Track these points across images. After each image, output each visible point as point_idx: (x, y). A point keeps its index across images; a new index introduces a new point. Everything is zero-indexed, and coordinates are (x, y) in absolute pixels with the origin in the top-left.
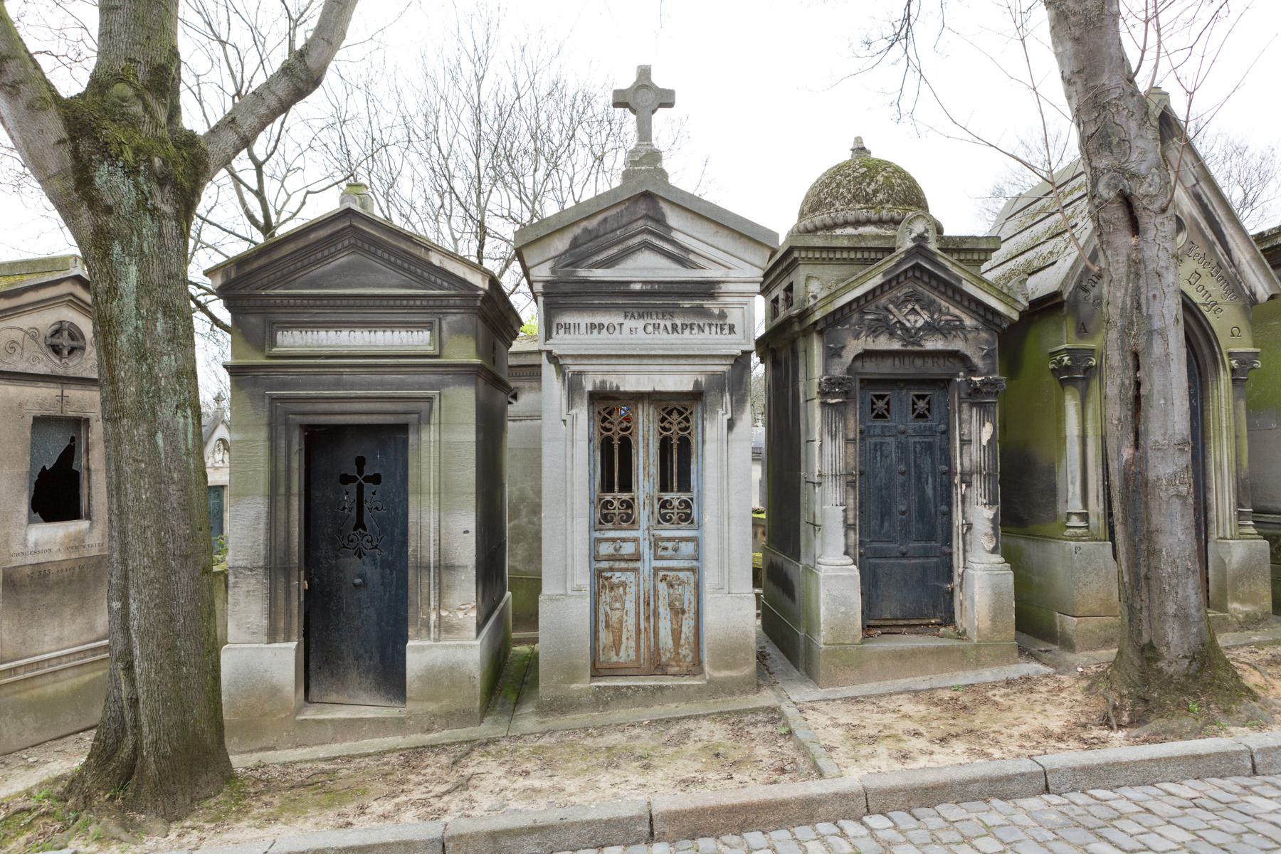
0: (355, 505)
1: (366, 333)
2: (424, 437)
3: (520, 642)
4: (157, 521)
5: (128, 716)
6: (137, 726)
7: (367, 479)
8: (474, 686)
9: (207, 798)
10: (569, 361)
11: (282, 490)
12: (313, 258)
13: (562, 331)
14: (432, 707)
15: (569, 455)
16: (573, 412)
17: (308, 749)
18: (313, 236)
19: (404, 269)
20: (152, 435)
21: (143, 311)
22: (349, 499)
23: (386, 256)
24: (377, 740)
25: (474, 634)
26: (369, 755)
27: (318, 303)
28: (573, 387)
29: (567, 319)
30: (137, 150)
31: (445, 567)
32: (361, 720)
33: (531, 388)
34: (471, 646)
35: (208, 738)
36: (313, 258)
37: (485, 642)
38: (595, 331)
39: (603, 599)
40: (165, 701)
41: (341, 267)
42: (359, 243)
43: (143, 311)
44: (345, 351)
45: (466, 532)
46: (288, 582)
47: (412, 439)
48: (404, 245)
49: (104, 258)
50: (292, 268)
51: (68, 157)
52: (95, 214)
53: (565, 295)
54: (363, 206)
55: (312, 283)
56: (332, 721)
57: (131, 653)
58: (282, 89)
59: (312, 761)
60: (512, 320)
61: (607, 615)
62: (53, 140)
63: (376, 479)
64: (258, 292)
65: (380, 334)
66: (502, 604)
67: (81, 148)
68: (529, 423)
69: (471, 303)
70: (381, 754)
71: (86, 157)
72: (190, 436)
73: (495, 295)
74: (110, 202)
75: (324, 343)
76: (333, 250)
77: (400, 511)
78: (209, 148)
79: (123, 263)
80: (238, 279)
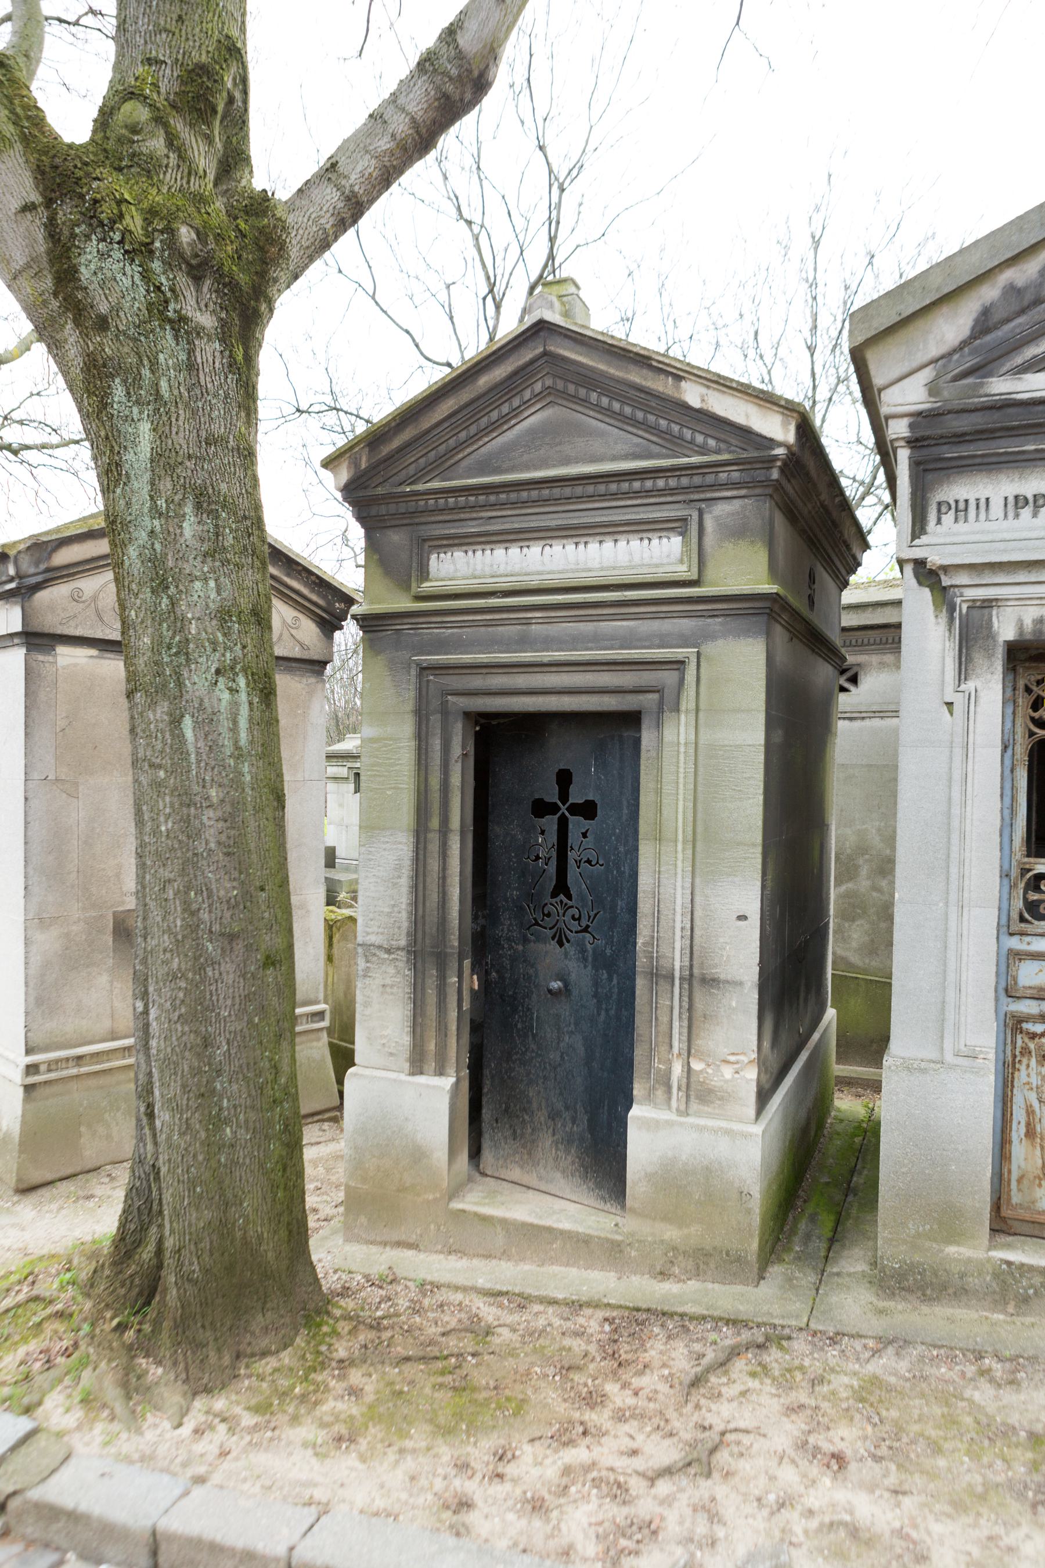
0: (554, 854)
1: (570, 547)
2: (669, 734)
3: (847, 1083)
4: (183, 872)
7: (575, 809)
8: (749, 1211)
9: (264, 1354)
10: (962, 579)
11: (435, 823)
13: (948, 518)
14: (671, 1233)
15: (957, 775)
16: (970, 686)
17: (463, 1263)
18: (484, 381)
20: (176, 722)
21: (161, 503)
22: (545, 843)
23: (605, 401)
24: (574, 1271)
25: (751, 1111)
26: (553, 1302)
27: (492, 498)
28: (970, 634)
29: (962, 489)
30: (151, 214)
32: (549, 1230)
33: (882, 665)
34: (746, 1136)
35: (270, 1251)
37: (776, 1124)
38: (1026, 512)
39: (1021, 1076)
40: (192, 1184)
41: (532, 432)
42: (560, 385)
43: (161, 503)
44: (535, 582)
45: (742, 918)
46: (442, 978)
47: (647, 737)
48: (636, 376)
49: (100, 412)
50: (452, 442)
51: (40, 235)
52: (85, 335)
53: (960, 438)
54: (566, 314)
55: (483, 468)
56: (504, 1222)
58: (417, 103)
59: (465, 1289)
60: (849, 532)
61: (1030, 1112)
62: (15, 204)
63: (588, 810)
64: (400, 489)
65: (593, 546)
66: (816, 1036)
67: (60, 217)
68: (877, 723)
69: (760, 475)
70: (576, 1306)
71: (66, 232)
72: (243, 723)
73: (811, 464)
74: (103, 308)
75: (502, 570)
76: (516, 402)
77: (626, 869)
78: (290, 219)
79: (128, 419)
80: (374, 468)
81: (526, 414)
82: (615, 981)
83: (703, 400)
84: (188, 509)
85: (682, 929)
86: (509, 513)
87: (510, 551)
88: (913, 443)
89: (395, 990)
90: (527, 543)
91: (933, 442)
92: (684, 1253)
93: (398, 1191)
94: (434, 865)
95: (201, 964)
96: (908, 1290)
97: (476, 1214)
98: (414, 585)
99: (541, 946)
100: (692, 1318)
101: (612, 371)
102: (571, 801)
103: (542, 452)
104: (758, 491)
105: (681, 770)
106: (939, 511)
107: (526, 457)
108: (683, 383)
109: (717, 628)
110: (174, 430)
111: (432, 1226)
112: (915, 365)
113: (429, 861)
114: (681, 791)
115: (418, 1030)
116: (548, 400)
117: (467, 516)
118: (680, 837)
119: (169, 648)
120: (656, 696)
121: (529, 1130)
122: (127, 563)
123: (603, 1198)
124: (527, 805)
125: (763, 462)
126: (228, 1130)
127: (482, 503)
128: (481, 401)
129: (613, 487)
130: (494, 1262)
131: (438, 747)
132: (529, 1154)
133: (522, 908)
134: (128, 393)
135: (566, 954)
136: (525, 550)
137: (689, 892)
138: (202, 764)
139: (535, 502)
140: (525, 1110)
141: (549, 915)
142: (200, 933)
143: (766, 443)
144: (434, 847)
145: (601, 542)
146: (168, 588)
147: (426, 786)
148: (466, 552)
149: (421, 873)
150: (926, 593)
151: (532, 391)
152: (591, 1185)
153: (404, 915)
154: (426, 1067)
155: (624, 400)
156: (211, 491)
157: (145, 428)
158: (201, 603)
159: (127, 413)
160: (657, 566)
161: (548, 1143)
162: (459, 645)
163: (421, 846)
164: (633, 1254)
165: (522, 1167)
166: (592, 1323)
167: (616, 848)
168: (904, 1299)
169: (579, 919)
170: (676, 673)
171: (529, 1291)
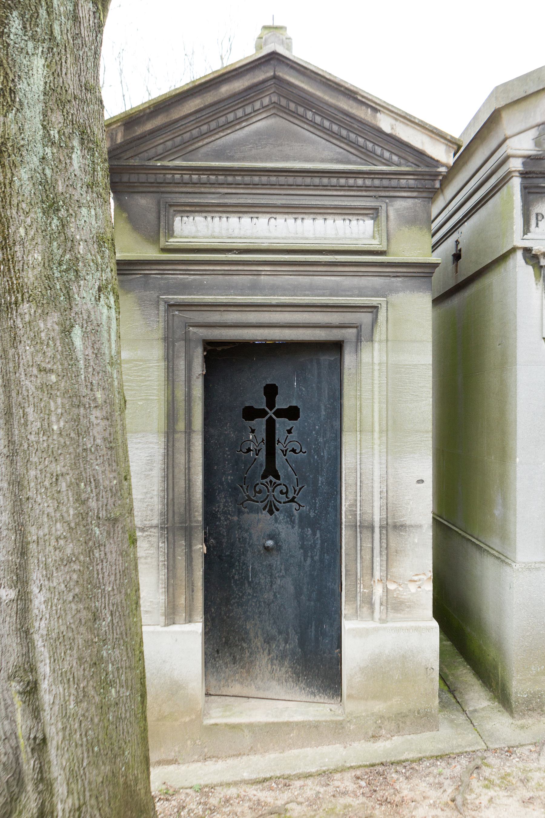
0: (264, 447)
1: (290, 220)
2: (365, 356)
4: (75, 466)
5: (29, 765)
6: (44, 780)
7: (280, 413)
8: (432, 681)
11: (181, 426)
12: (222, 120)
14: (379, 707)
17: (220, 765)
18: (226, 90)
19: (340, 138)
20: (67, 331)
21: (54, 133)
23: (318, 119)
24: (309, 751)
26: (309, 776)
27: (230, 179)
31: (394, 527)
36: (222, 120)
40: (90, 746)
41: (258, 133)
42: (283, 102)
44: (265, 245)
45: (421, 481)
46: (189, 546)
47: (348, 359)
48: (345, 104)
50: (195, 132)
55: (219, 155)
56: (250, 726)
57: (33, 669)
59: (236, 784)
63: (292, 413)
64: (151, 163)
69: (428, 184)
70: (326, 775)
76: (249, 109)
80: (127, 145)
81: (254, 120)
82: (318, 535)
83: (392, 128)
84: (76, 143)
85: (381, 492)
86: (242, 191)
87: (243, 220)
88: (524, 175)
89: (149, 560)
90: (256, 215)
91: (535, 176)
92: (388, 718)
93: (158, 720)
94: (181, 459)
95: (90, 547)
96: (533, 710)
97: (226, 725)
98: (162, 239)
99: (253, 516)
100: (413, 761)
101: (327, 98)
102: (277, 407)
103: (267, 149)
104: (424, 195)
105: (376, 382)
106: (537, 219)
107: (254, 152)
108: (378, 114)
109: (399, 284)
110: (64, 71)
111: (189, 742)
112: (528, 125)
113: (177, 455)
114: (376, 396)
115: (171, 590)
116: (272, 112)
117: (207, 190)
118: (377, 428)
119: (60, 265)
120: (354, 331)
121: (248, 654)
122: (17, 183)
123: (313, 694)
124: (239, 412)
125: (431, 175)
126: (113, 690)
127: (220, 182)
128: (222, 104)
129: (325, 181)
130: (244, 758)
131: (183, 367)
132: (248, 672)
133: (236, 489)
134: (25, 28)
135: (276, 520)
136: (255, 220)
137: (384, 466)
138: (90, 370)
139: (264, 185)
140: (243, 639)
141: (260, 492)
142: (89, 519)
143: (435, 163)
144: (181, 444)
145: (314, 219)
146: (58, 210)
147: (173, 397)
148: (206, 217)
149: (170, 466)
150: (530, 269)
151: (262, 103)
152: (303, 685)
153: (156, 500)
154: (177, 618)
155: (333, 120)
156: (89, 131)
157: (39, 62)
158: (87, 228)
159: (22, 45)
160: (356, 239)
161: (264, 662)
162: (200, 288)
163: (170, 444)
164: (352, 727)
165: (242, 684)
166: (347, 783)
168: (530, 716)
169: (287, 493)
170: (370, 315)
171: (287, 772)
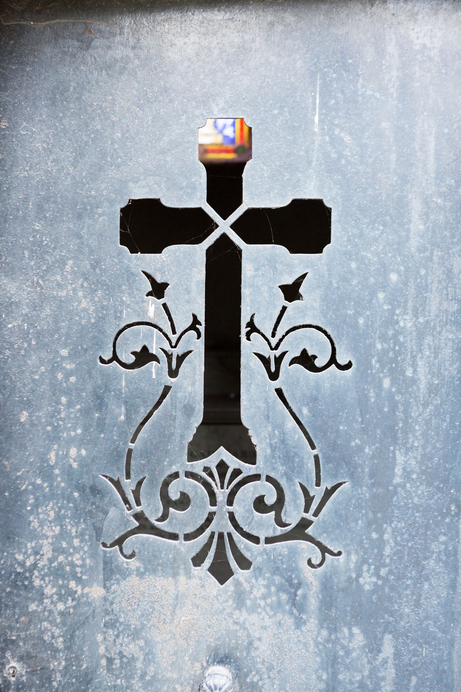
77: (232, 396)
82: (388, 650)
141: (184, 502)
167: (390, 321)
